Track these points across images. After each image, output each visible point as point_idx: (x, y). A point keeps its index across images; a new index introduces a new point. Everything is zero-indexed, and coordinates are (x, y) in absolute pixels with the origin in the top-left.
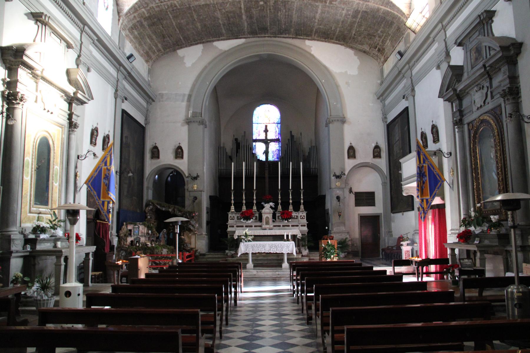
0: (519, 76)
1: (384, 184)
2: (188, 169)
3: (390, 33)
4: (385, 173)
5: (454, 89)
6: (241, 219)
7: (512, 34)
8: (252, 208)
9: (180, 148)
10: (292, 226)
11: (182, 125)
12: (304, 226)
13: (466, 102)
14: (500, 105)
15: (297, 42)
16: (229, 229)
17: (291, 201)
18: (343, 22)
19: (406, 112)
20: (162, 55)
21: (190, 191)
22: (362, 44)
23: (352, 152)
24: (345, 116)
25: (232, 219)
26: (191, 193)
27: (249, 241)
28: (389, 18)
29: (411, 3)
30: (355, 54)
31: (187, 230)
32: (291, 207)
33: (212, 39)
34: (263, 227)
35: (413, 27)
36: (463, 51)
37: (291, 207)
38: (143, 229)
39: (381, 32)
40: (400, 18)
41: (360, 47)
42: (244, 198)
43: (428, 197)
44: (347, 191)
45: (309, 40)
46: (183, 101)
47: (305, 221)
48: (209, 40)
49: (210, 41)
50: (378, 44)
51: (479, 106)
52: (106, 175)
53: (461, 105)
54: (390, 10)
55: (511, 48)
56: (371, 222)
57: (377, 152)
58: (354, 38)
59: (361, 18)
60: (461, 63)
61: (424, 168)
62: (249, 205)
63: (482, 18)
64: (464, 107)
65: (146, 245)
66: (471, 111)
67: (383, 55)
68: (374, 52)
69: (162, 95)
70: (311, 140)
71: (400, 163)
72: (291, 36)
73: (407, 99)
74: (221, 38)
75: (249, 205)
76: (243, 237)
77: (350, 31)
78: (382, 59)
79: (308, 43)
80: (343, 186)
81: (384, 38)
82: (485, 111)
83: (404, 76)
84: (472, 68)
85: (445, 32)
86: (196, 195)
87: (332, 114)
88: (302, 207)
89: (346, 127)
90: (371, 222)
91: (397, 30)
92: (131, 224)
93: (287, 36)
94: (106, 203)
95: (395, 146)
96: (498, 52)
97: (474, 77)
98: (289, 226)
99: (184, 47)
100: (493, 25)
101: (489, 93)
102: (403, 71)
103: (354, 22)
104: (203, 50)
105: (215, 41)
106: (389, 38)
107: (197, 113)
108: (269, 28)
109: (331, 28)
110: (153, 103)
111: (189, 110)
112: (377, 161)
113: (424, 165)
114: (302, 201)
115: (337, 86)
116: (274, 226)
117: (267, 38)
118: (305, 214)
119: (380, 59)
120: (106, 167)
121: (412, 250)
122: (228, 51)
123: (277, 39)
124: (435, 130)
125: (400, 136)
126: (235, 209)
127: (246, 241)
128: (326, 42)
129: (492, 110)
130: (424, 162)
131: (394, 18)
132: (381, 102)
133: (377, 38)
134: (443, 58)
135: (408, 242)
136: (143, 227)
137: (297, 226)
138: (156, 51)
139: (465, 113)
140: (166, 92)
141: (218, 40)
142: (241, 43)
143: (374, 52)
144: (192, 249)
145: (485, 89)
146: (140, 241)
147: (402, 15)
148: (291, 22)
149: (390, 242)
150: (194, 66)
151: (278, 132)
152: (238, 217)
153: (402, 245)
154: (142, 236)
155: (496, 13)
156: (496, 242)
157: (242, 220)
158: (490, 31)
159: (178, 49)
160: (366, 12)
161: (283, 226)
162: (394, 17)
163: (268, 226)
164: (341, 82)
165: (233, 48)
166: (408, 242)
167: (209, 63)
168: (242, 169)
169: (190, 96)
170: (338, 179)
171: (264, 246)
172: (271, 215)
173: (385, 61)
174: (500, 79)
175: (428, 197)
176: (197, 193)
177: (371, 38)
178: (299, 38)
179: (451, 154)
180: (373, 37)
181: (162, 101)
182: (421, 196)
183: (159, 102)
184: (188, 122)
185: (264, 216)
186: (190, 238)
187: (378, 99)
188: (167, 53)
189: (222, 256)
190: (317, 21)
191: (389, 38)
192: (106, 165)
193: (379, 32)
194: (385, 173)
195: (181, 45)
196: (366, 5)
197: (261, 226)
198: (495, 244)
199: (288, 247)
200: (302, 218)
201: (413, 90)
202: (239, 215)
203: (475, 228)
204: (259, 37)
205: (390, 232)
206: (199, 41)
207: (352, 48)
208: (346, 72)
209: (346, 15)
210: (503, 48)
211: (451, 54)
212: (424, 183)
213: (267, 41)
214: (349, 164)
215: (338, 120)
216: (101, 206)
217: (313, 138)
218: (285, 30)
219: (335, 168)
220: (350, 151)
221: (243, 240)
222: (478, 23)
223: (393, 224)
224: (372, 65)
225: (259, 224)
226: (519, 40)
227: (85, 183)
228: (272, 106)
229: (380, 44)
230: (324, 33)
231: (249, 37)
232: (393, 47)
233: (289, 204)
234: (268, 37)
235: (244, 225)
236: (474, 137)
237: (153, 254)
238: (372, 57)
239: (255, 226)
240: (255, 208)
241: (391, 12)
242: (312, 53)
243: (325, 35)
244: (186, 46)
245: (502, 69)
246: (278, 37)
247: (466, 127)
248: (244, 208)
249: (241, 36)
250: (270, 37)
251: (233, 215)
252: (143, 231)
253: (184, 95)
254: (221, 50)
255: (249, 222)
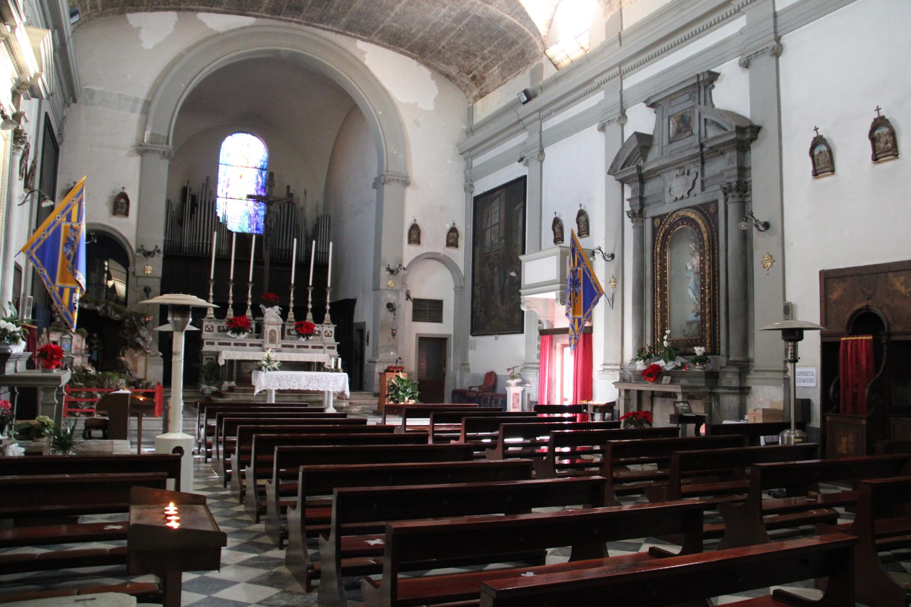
0: (750, 168)
1: (458, 289)
2: (137, 237)
3: (504, 56)
4: (462, 269)
5: (633, 165)
6: (227, 331)
7: (745, 111)
8: (305, 318)
9: (124, 196)
10: (313, 347)
11: (130, 155)
12: (333, 348)
13: (651, 187)
14: (716, 202)
15: (342, 41)
16: (206, 348)
17: (310, 306)
18: (435, 24)
19: (523, 182)
20: (96, 16)
21: (137, 277)
22: (448, 63)
23: (415, 234)
24: (409, 174)
25: (209, 331)
26: (139, 280)
27: (275, 369)
28: (512, 35)
29: (552, 20)
30: (433, 78)
31: (131, 346)
32: (310, 316)
33: (196, 7)
34: (266, 346)
35: (557, 59)
36: (655, 115)
37: (310, 316)
38: (78, 341)
39: (490, 52)
40: (530, 39)
41: (444, 67)
42: (231, 295)
43: (581, 316)
44: (403, 296)
45: (362, 40)
46: (133, 110)
47: (331, 340)
48: (191, 7)
49: (192, 10)
50: (476, 69)
51: (679, 196)
52: (68, 239)
53: (642, 190)
54: (518, 24)
55: (748, 130)
56: (434, 349)
57: (452, 238)
58: (439, 52)
59: (467, 25)
60: (650, 132)
61: (578, 274)
62: (240, 308)
63: (701, 79)
64: (646, 194)
65: (86, 371)
66: (661, 201)
67: (477, 87)
68: (464, 79)
69: (92, 93)
70: (317, 205)
71: (521, 261)
72: (336, 29)
73: (526, 164)
74: (214, 8)
75: (240, 308)
76: (265, 363)
77: (438, 40)
78: (476, 92)
79: (361, 45)
80: (398, 287)
81: (491, 62)
82: (688, 205)
83: (524, 128)
84: (670, 142)
85: (622, 80)
86: (147, 285)
87: (390, 169)
88: (327, 316)
89: (409, 191)
90: (434, 349)
91: (519, 55)
92: (58, 331)
93: (329, 27)
94: (67, 292)
95: (488, 232)
96: (731, 133)
97: (679, 157)
98: (307, 347)
99: (141, 11)
100: (713, 91)
101: (698, 182)
102: (525, 121)
103: (453, 29)
104: (176, 22)
105: (202, 11)
106: (500, 63)
107: (159, 136)
108: (306, 9)
109: (411, 29)
110: (73, 105)
111: (145, 130)
112: (451, 252)
113: (579, 269)
114: (310, 306)
115: (401, 125)
116: (284, 346)
117: (293, 25)
118: (332, 328)
119: (471, 92)
120: (69, 224)
121: (523, 392)
122: (224, 34)
123: (310, 29)
124: (583, 220)
125: (503, 217)
126: (295, 317)
127: (269, 370)
128: (389, 48)
129: (700, 205)
130: (579, 265)
131: (520, 36)
132: (465, 159)
133: (478, 59)
134: (616, 116)
135: (518, 380)
136: (79, 337)
137: (321, 347)
138: (88, 7)
139: (647, 201)
140: (101, 88)
141: (209, 11)
142: (247, 24)
143: (464, 79)
144: (140, 381)
145: (693, 176)
146: (72, 363)
147: (535, 35)
148: (350, 7)
149: (466, 380)
150: (154, 51)
151: (260, 184)
152: (219, 327)
153: (509, 385)
154: (76, 354)
155: (719, 77)
156: (701, 383)
157: (229, 333)
158: (708, 99)
159: (130, 11)
160: (479, 18)
161: (299, 347)
162: (521, 35)
163: (273, 346)
164: (407, 118)
165: (232, 31)
166: (518, 380)
167: (188, 50)
168: (211, 245)
169: (148, 104)
170: (391, 276)
171: (298, 379)
172: (280, 327)
173: (481, 96)
174: (722, 167)
175: (581, 316)
176: (151, 280)
177: (468, 57)
178: (347, 35)
179: (613, 256)
180: (472, 57)
181: (92, 105)
182: (574, 313)
183: (86, 104)
184: (142, 150)
185: (268, 329)
186: (135, 361)
187: (461, 154)
188: (107, 15)
189: (193, 394)
190: (392, 14)
191: (500, 63)
192: (69, 218)
193: (486, 51)
194: (462, 269)
195: (138, 6)
196: (486, 8)
197: (260, 345)
198: (700, 385)
199: (336, 381)
200: (328, 336)
201: (542, 152)
202: (224, 324)
203: (666, 362)
204: (280, 20)
205: (465, 365)
206: (172, 6)
207: (428, 65)
208: (416, 104)
209: (444, 16)
210: (740, 130)
211: (627, 113)
212: (576, 295)
213: (294, 29)
214: (410, 252)
215: (398, 180)
216: (58, 295)
217: (321, 202)
218: (332, 18)
219: (387, 257)
220: (413, 232)
221: (263, 368)
222: (694, 84)
223: (471, 353)
224: (456, 98)
225: (258, 341)
226: (757, 123)
227: (23, 250)
228: (249, 135)
229: (480, 68)
230: (395, 35)
231: (264, 17)
232: (503, 78)
233: (307, 310)
234: (297, 22)
235: (232, 343)
236: (665, 238)
237: (102, 387)
238: (459, 86)
239: (251, 345)
240: (249, 313)
241: (518, 27)
242: (366, 63)
243: (395, 40)
244: (146, 10)
245: (728, 155)
246: (313, 26)
247: (648, 223)
248: (230, 313)
249: (250, 13)
250: (300, 23)
251: (212, 323)
252: (79, 346)
253: (136, 100)
254: (211, 30)
255: (242, 336)
